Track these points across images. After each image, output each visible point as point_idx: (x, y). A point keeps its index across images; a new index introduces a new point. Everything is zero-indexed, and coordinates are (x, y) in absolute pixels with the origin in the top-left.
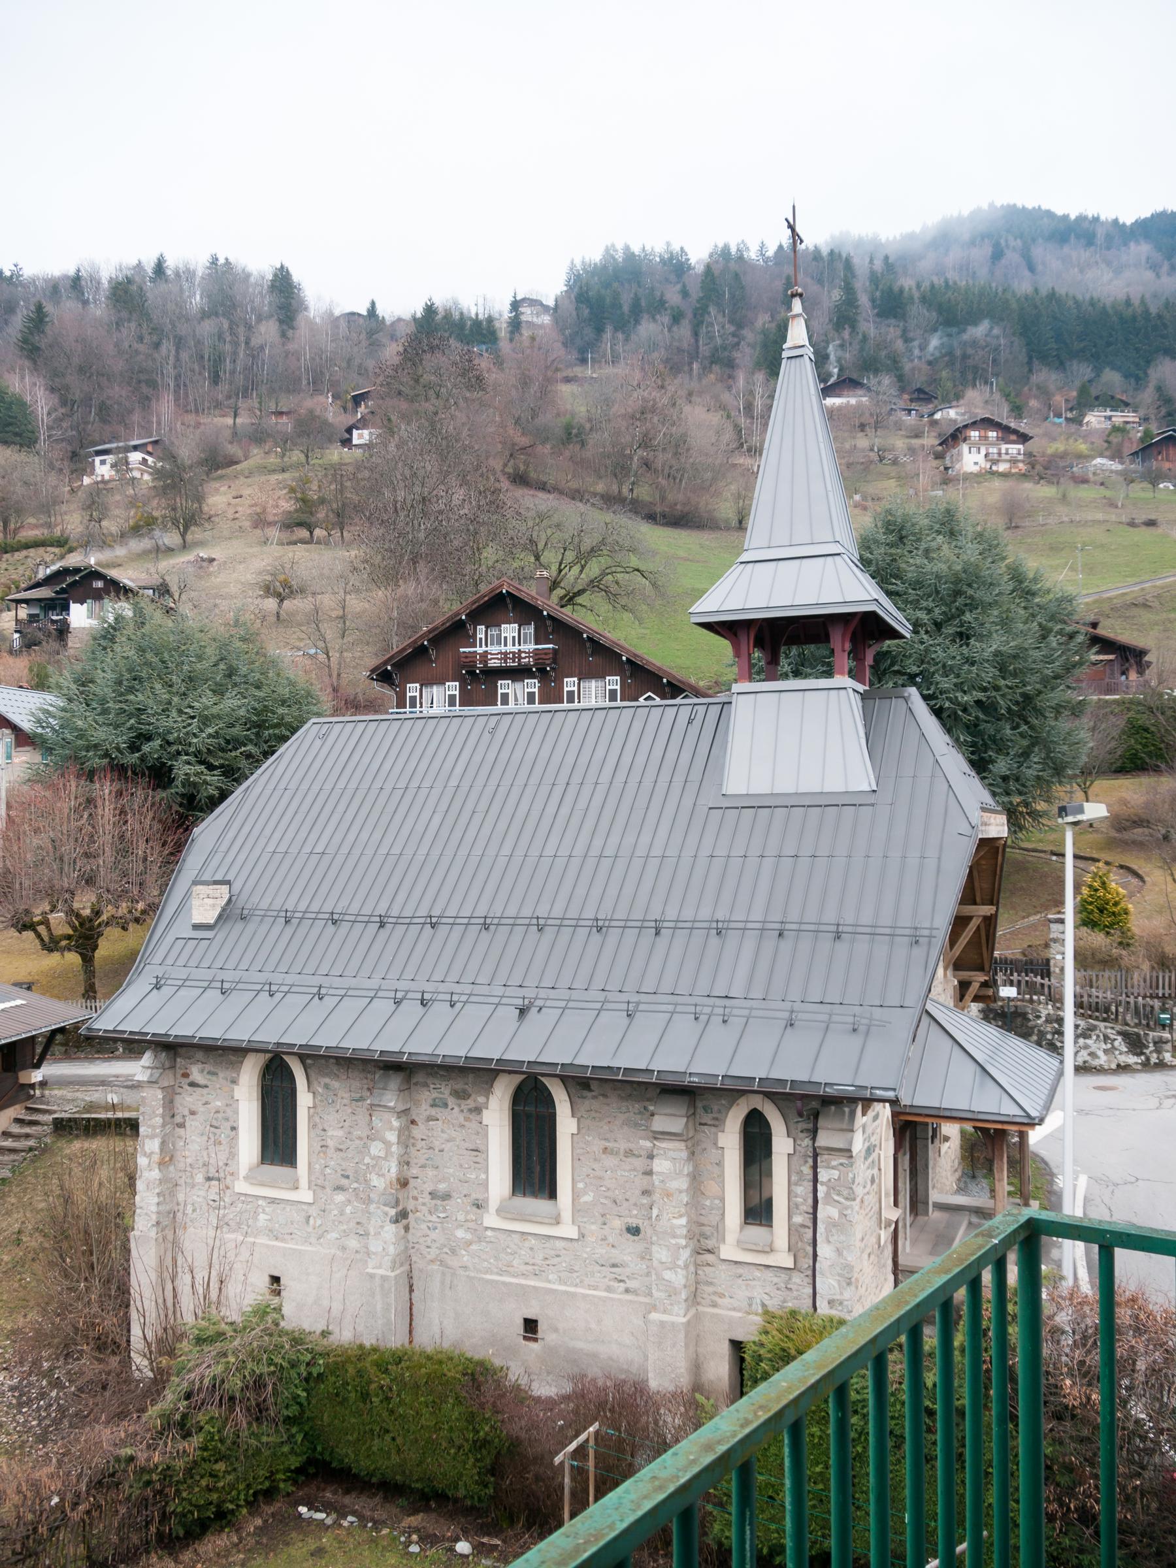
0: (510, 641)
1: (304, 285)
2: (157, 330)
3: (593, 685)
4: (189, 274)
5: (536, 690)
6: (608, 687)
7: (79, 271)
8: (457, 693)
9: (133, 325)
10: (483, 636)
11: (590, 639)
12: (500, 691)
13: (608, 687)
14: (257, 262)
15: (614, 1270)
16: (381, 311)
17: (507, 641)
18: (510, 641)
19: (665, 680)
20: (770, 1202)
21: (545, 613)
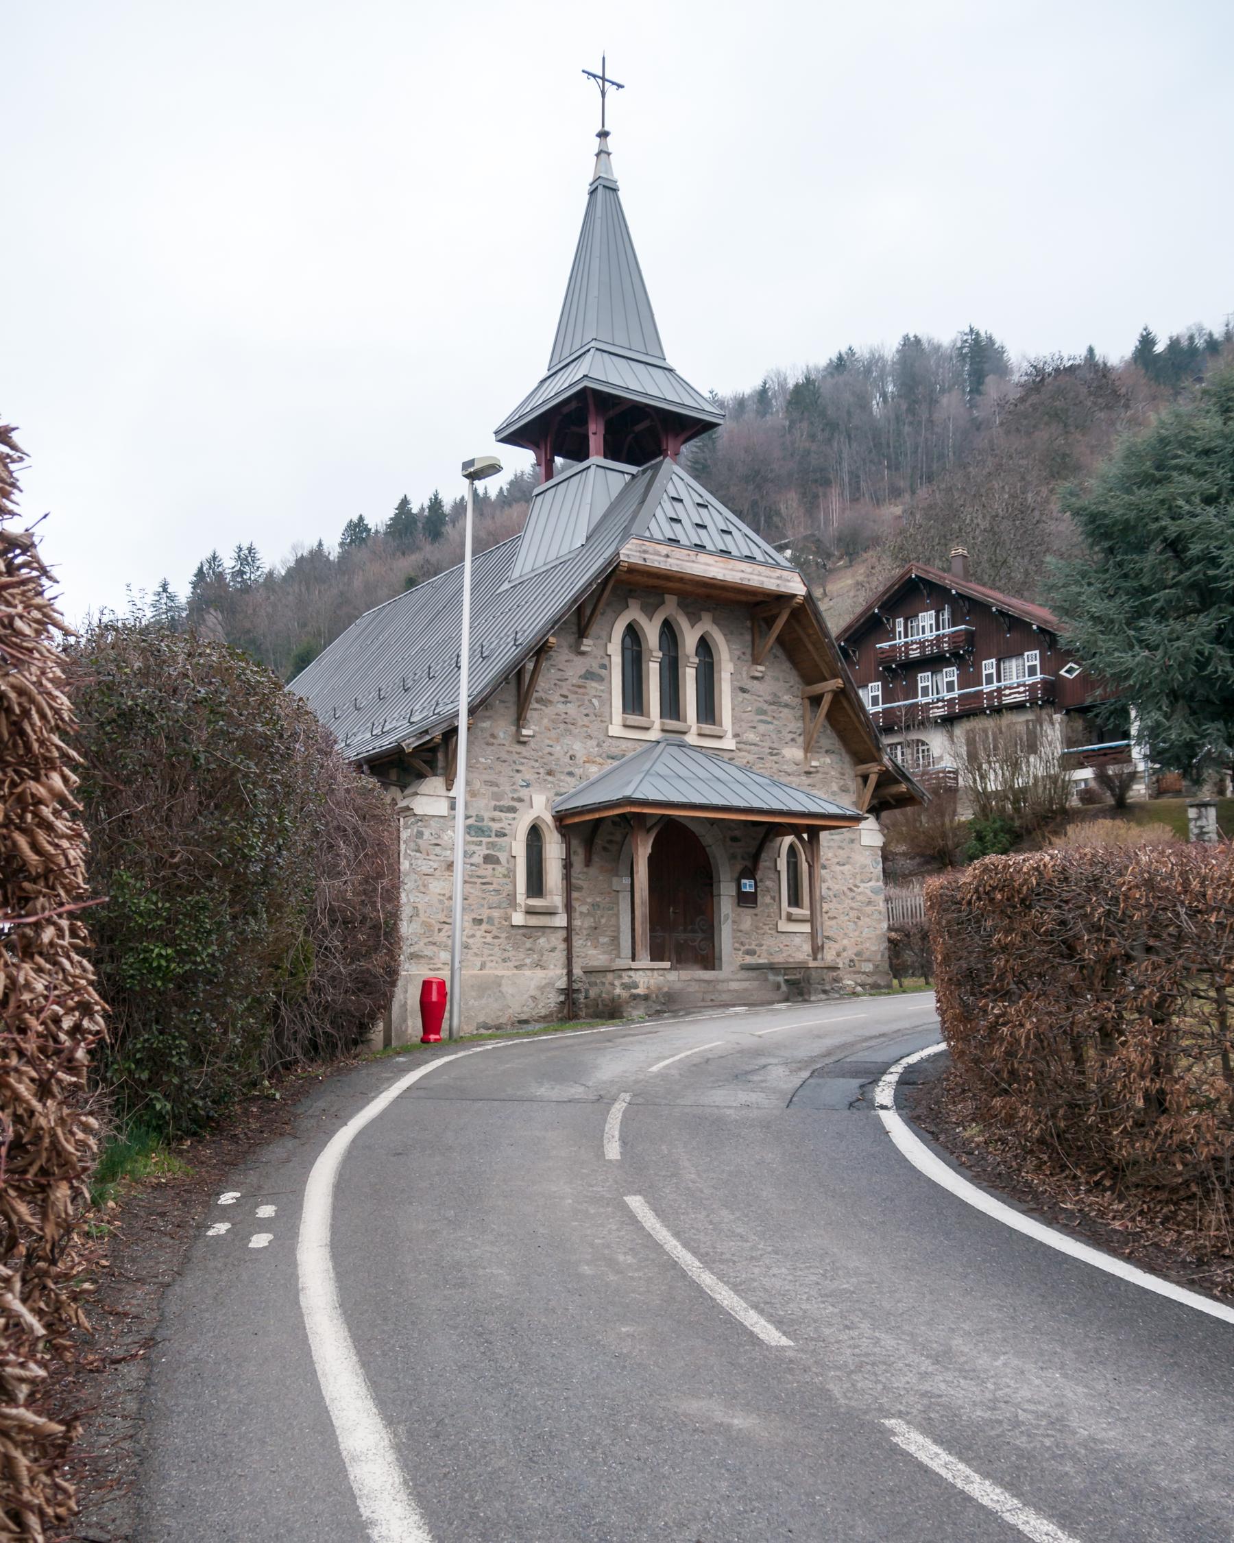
0: (927, 629)
1: (1008, 347)
2: (832, 426)
3: (1013, 665)
4: (875, 361)
5: (955, 678)
6: (1027, 664)
7: (765, 383)
8: (880, 693)
9: (805, 425)
10: (902, 629)
11: (1000, 612)
12: (920, 685)
13: (1027, 664)
14: (945, 333)
15: (484, 887)
16: (1099, 356)
17: (926, 628)
18: (927, 629)
19: (1035, 627)
20: (457, 727)
21: (954, 592)
